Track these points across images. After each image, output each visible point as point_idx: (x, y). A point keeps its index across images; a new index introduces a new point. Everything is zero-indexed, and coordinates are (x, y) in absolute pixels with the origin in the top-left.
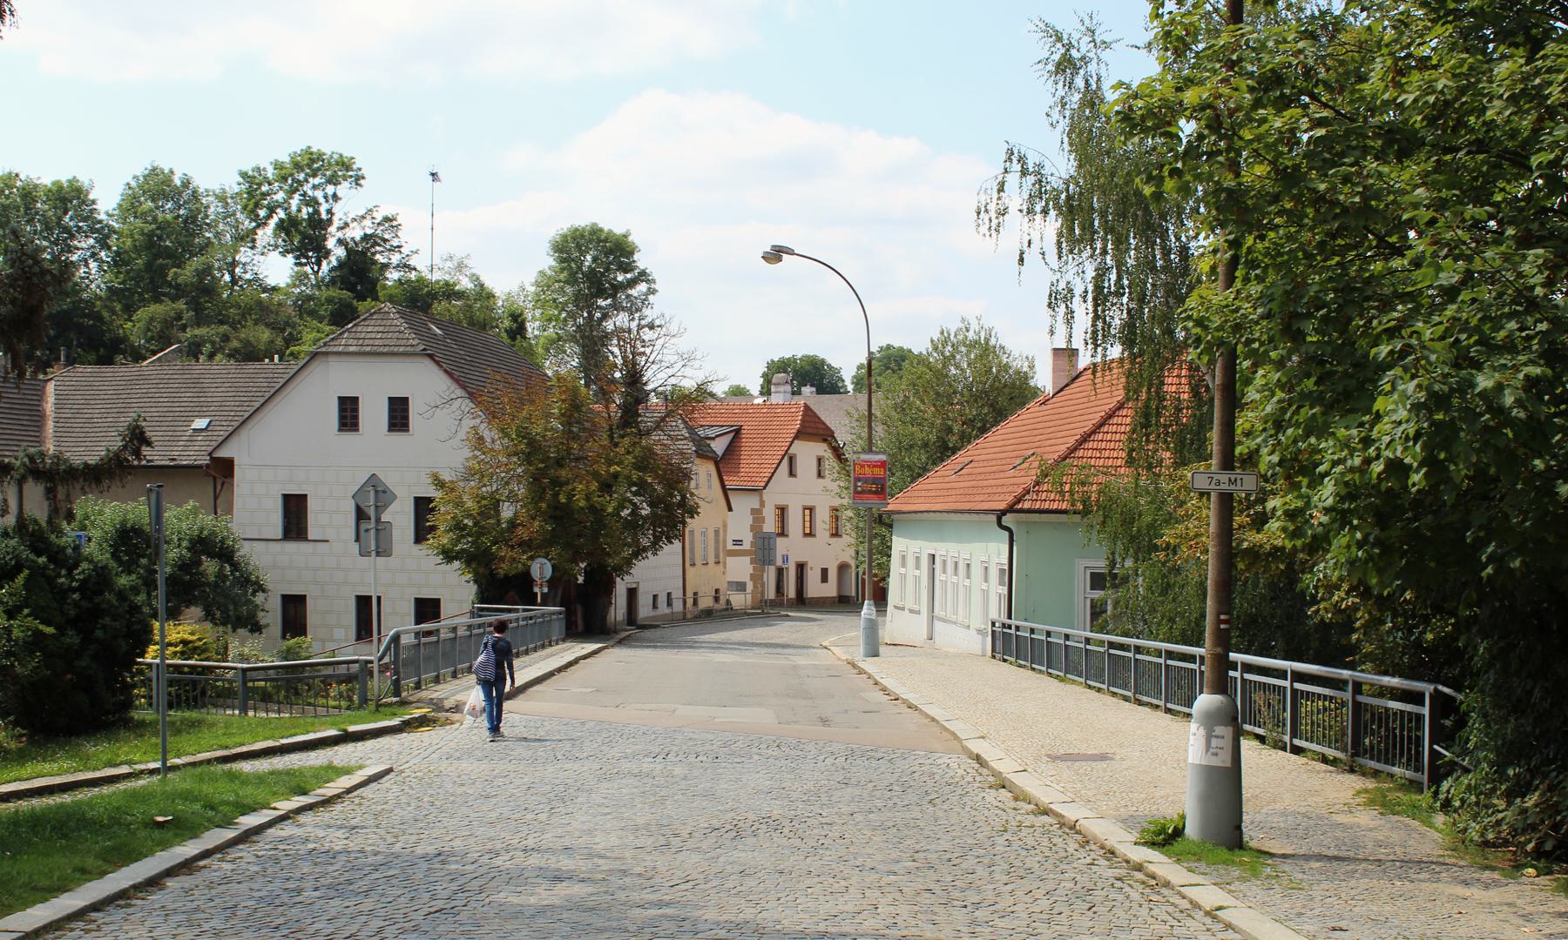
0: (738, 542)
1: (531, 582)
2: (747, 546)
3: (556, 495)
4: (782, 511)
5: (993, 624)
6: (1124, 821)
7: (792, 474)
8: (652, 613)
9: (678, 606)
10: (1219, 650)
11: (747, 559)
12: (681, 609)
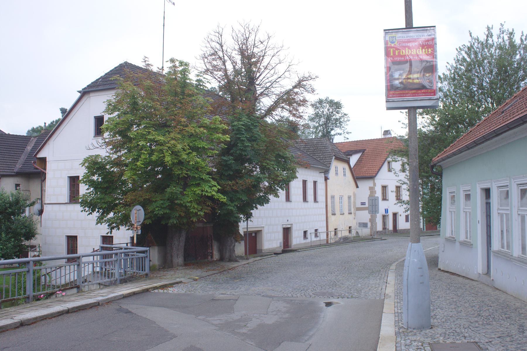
0: (363, 204)
2: (367, 205)
4: (384, 188)
6: (175, 336)
8: (303, 241)
9: (323, 237)
12: (325, 238)
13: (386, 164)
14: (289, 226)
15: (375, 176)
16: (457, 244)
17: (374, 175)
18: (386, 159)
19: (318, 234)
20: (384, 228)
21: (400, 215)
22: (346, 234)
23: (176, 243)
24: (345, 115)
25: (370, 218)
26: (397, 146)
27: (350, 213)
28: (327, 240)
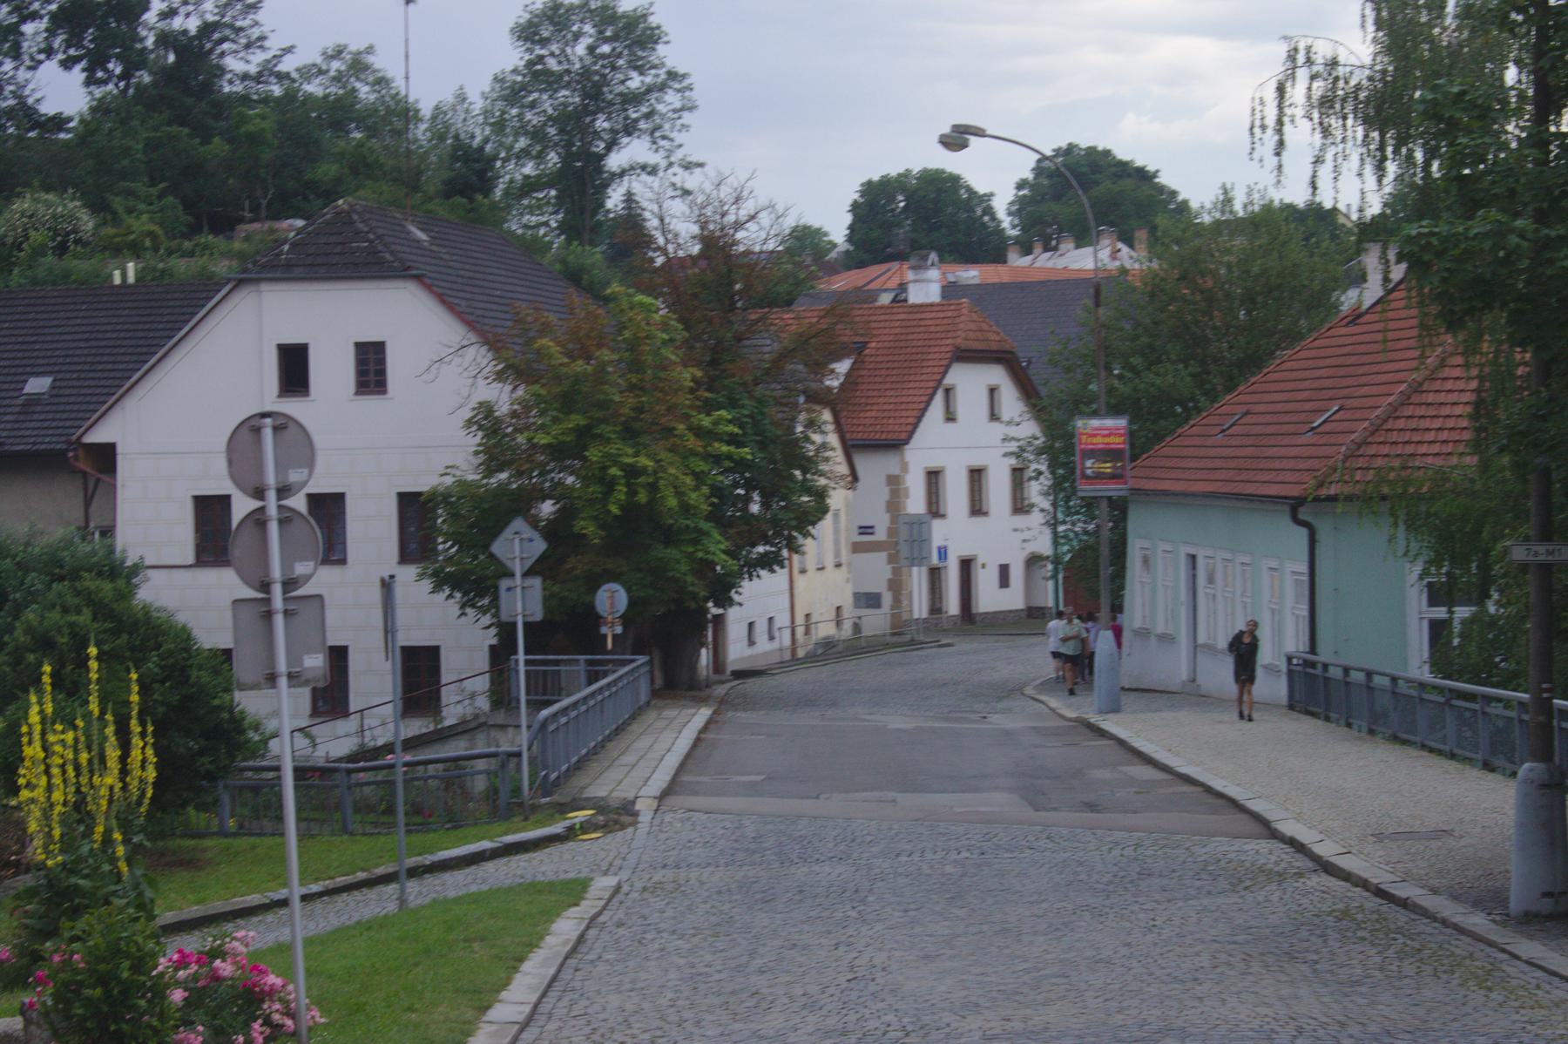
1: (597, 619)
2: (881, 535)
3: (632, 492)
4: (934, 477)
5: (1289, 659)
7: (950, 417)
8: (749, 652)
10: (1541, 718)
11: (882, 557)
12: (787, 641)
13: (939, 398)
14: (1425, 624)
15: (907, 441)
16: (1153, 640)
17: (904, 436)
18: (940, 382)
19: (777, 634)
20: (936, 608)
21: (983, 566)
22: (826, 630)
23: (33, 699)
24: (673, 75)
25: (889, 575)
26: (971, 335)
27: (838, 565)
28: (794, 651)
